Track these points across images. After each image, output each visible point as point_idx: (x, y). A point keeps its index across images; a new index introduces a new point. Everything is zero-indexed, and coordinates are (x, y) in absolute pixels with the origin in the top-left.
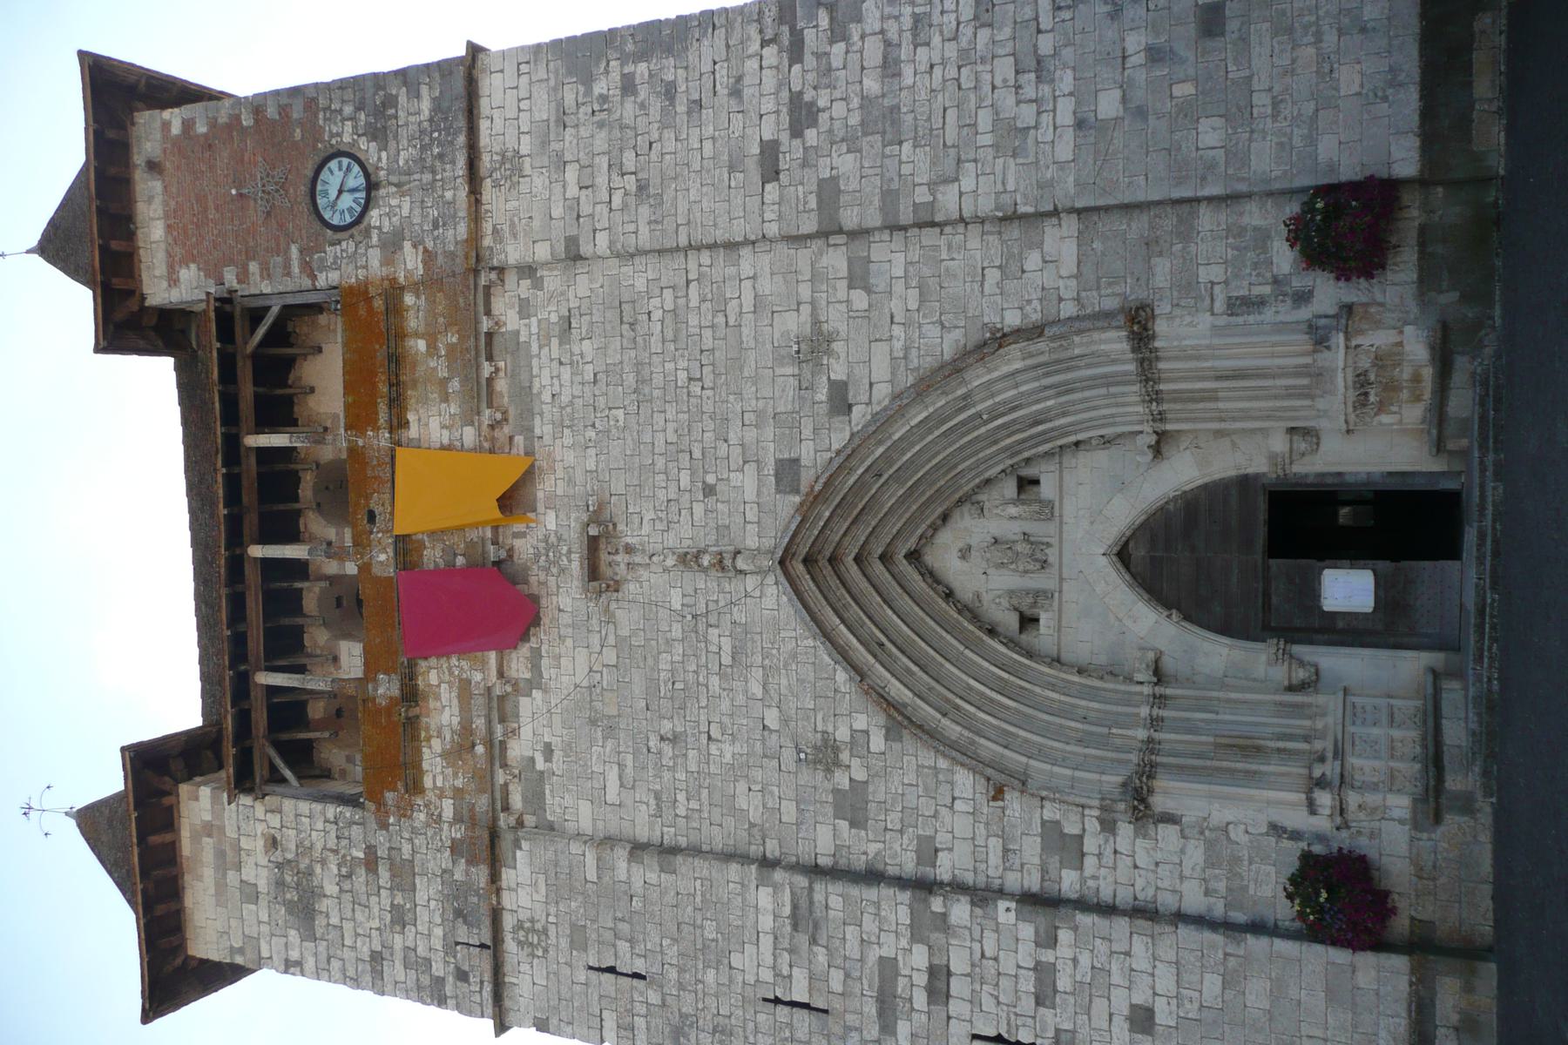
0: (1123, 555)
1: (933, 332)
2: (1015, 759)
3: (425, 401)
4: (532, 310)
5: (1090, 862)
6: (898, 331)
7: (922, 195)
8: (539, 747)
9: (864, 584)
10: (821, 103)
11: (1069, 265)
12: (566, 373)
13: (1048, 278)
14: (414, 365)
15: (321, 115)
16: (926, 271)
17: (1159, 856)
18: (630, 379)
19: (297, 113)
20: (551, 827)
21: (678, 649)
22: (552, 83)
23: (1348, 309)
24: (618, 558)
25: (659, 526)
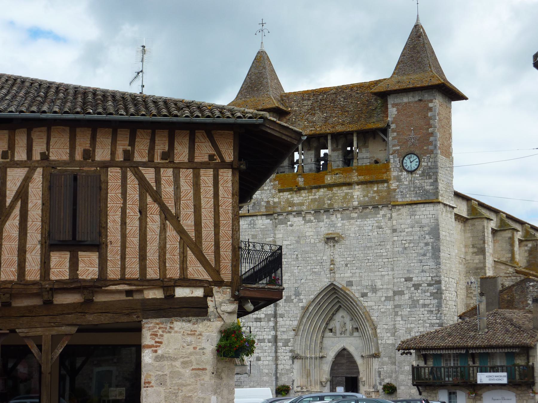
0: (344, 349)
1: (376, 315)
2: (300, 333)
3: (364, 190)
4: (384, 218)
5: (284, 348)
6: (377, 307)
7: (400, 313)
8: (293, 223)
9: (332, 299)
10: (419, 291)
11: (388, 342)
12: (370, 228)
13: (385, 338)
14: (371, 187)
15: (429, 155)
16: (388, 313)
17: (287, 361)
18: (369, 245)
19: (431, 147)
20: (276, 227)
21: (314, 258)
22: (430, 224)
23: (378, 392)
24: (332, 244)
25: (339, 253)
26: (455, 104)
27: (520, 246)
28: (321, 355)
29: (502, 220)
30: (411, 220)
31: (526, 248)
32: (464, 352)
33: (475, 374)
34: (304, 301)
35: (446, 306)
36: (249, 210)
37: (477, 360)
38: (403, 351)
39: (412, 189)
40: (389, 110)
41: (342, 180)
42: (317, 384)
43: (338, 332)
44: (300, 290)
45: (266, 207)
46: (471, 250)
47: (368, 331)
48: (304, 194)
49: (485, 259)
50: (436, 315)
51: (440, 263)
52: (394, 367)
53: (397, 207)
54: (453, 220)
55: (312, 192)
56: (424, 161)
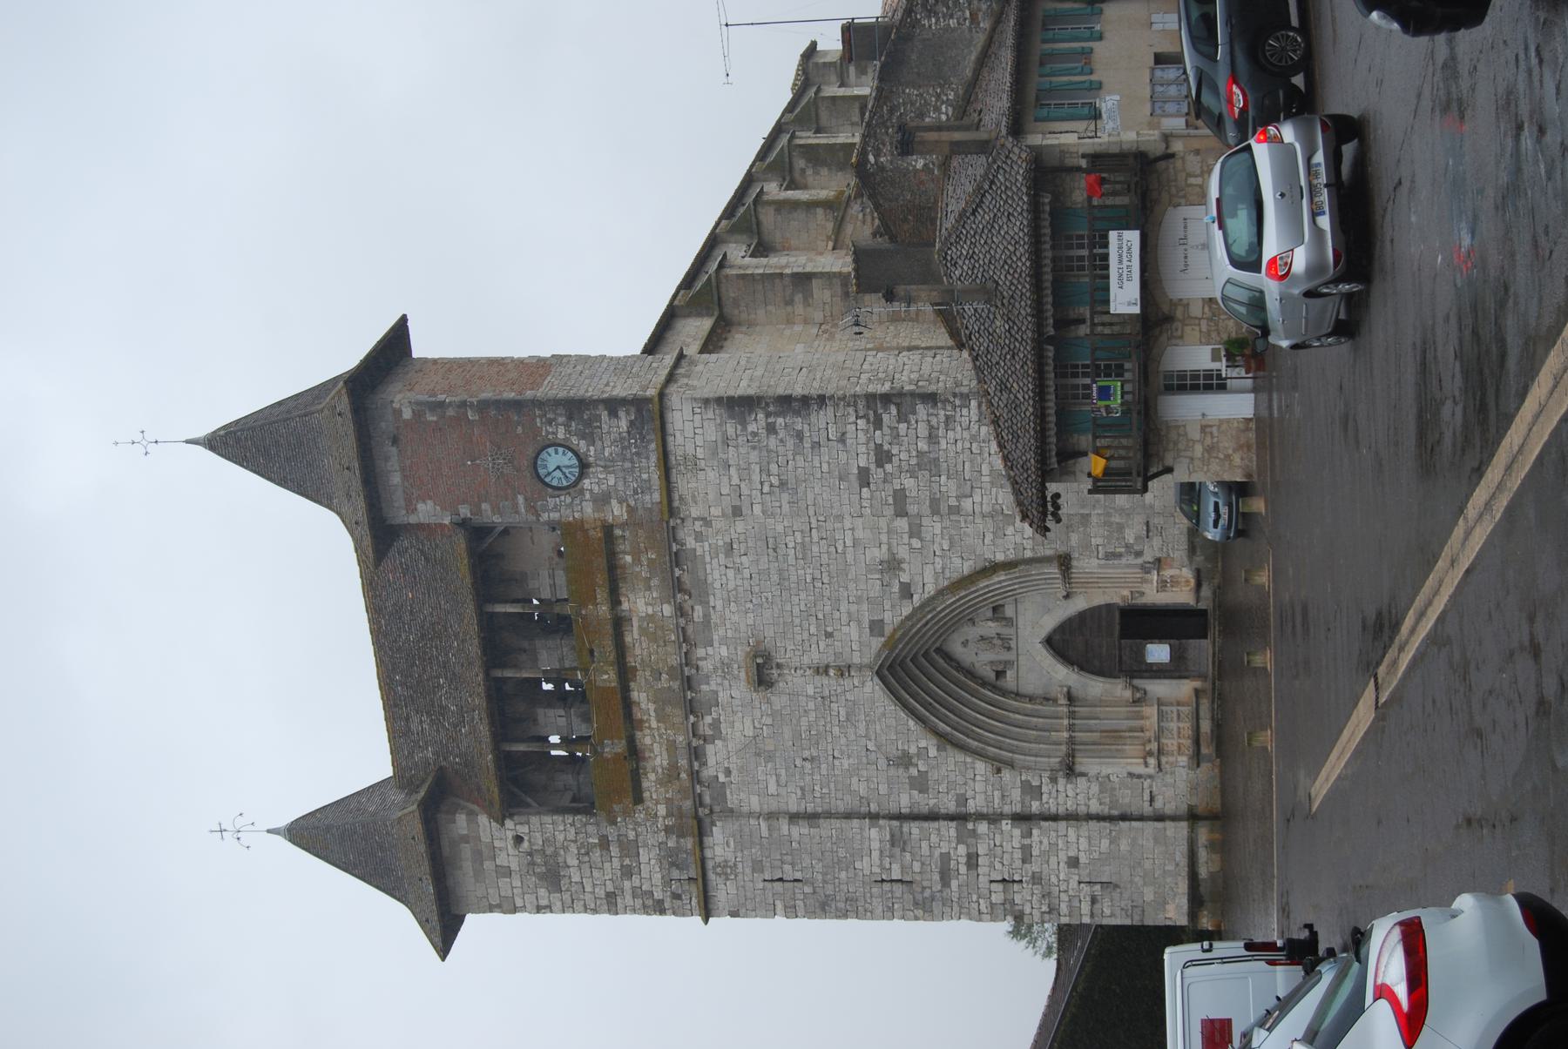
0: (1049, 642)
1: (957, 561)
4: (705, 538)
5: (1045, 797)
6: (938, 560)
7: (953, 502)
10: (894, 452)
12: (731, 573)
13: (1018, 539)
15: (538, 420)
16: (953, 532)
17: (1078, 791)
18: (775, 578)
20: (732, 811)
22: (718, 421)
24: (774, 671)
25: (796, 653)
26: (422, 346)
27: (805, 187)
28: (1063, 701)
29: (733, 230)
30: (709, 470)
31: (809, 172)
32: (1051, 348)
33: (1115, 320)
34: (925, 745)
35: (934, 380)
36: (690, 879)
37: (1072, 315)
38: (1050, 517)
39: (628, 465)
40: (422, 520)
41: (609, 643)
42: (1139, 712)
43: (1005, 656)
44: (893, 752)
45: (681, 835)
46: (799, 309)
47: (1000, 582)
48: (645, 739)
49: (821, 273)
50: (958, 410)
51: (819, 396)
52: (1094, 519)
53: (676, 504)
54: (714, 357)
55: (641, 721)
56: (553, 433)
